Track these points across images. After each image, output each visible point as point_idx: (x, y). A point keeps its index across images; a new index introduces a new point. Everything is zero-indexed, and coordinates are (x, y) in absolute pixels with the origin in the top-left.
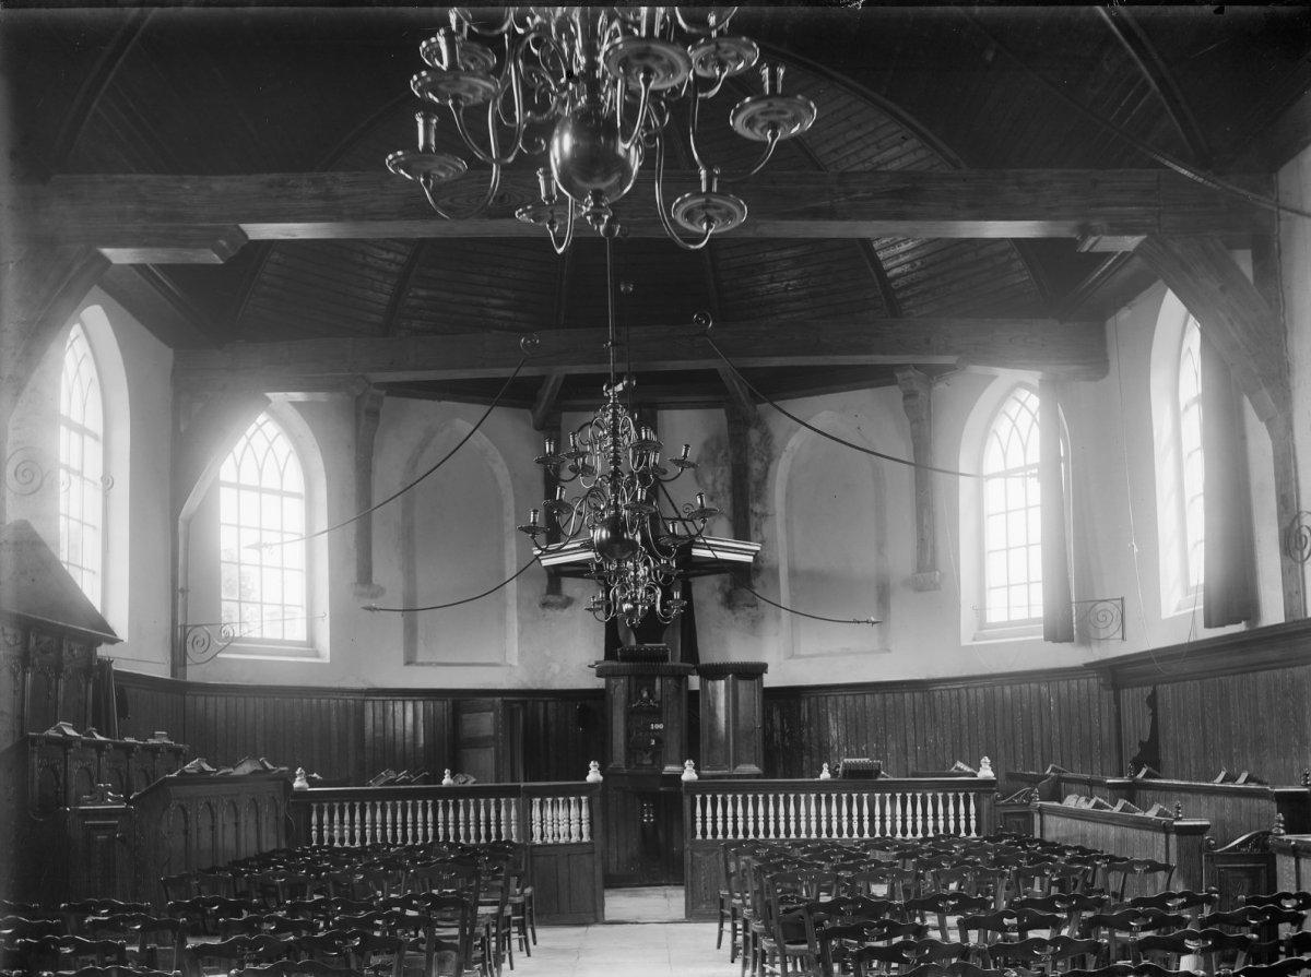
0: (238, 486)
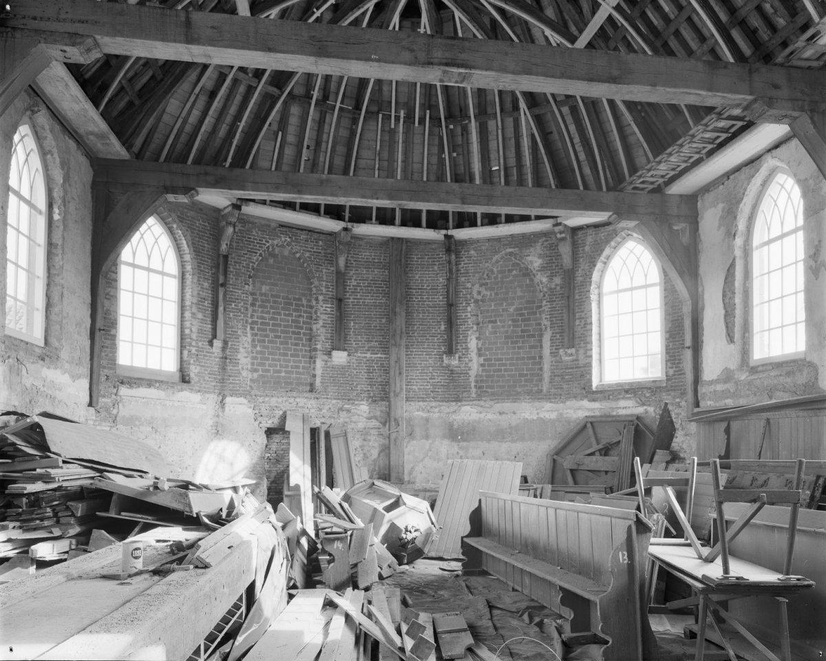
0: (134, 266)
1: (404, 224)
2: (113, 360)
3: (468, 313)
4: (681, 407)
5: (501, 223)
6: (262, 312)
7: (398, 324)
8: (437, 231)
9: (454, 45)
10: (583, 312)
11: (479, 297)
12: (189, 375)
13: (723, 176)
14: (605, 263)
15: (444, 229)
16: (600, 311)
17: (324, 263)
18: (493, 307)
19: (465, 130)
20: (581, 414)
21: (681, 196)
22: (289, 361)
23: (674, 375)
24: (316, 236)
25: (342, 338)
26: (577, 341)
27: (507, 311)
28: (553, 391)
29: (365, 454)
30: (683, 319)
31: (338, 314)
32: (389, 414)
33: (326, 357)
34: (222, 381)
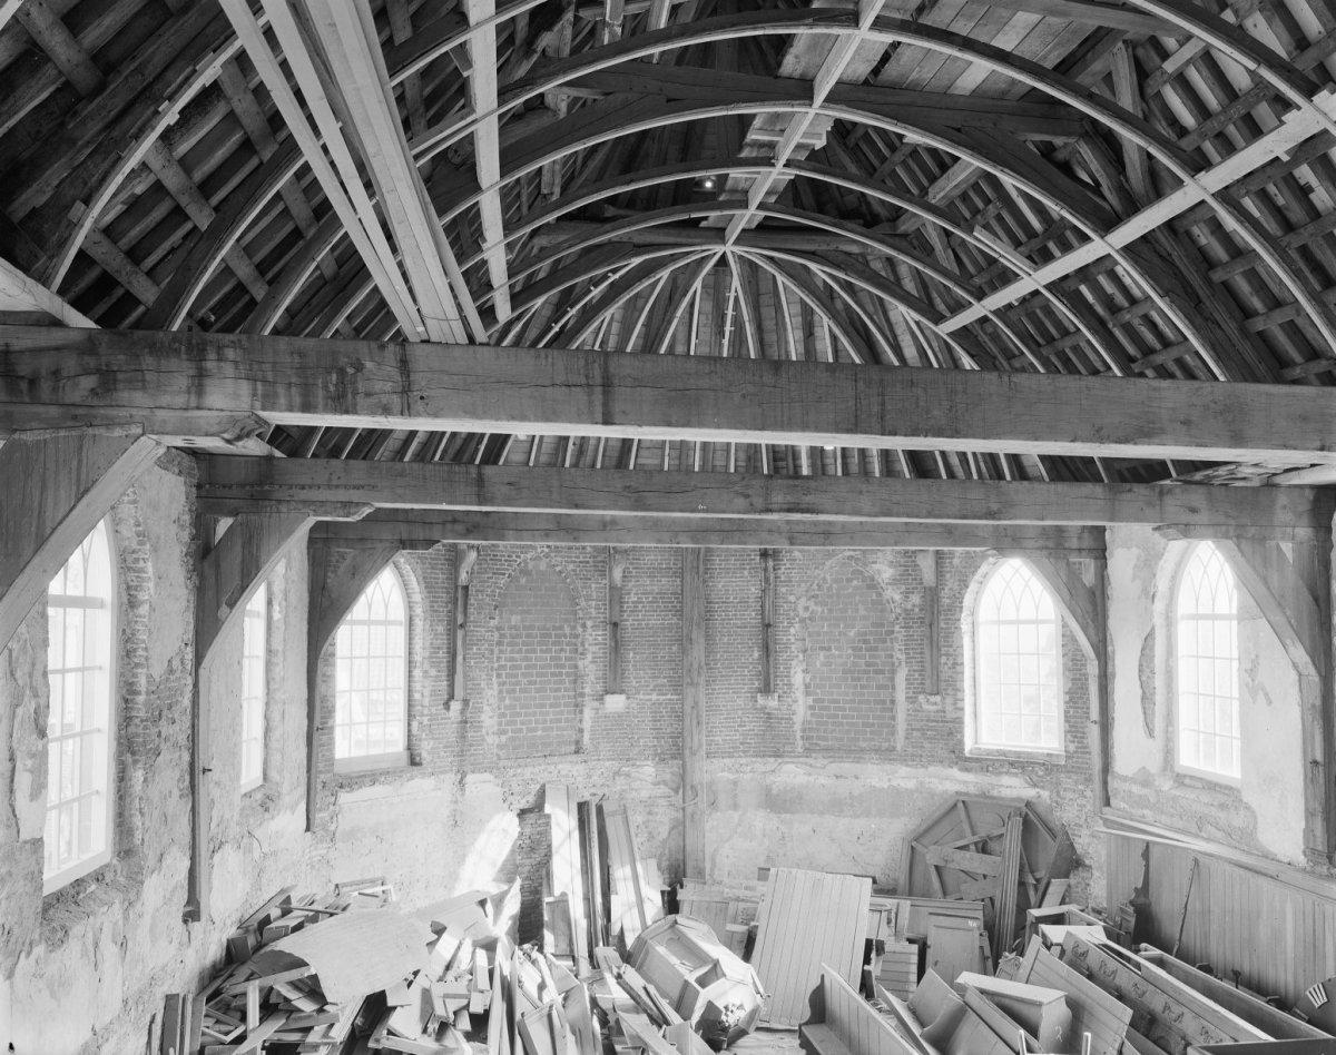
2: (331, 761)
3: (791, 635)
4: (1085, 797)
6: (512, 652)
7: (695, 654)
9: (797, 486)
10: (951, 646)
11: (807, 615)
12: (420, 755)
16: (974, 646)
18: (825, 629)
20: (951, 787)
22: (547, 713)
23: (1076, 752)
25: (619, 675)
26: (943, 685)
27: (845, 634)
28: (910, 750)
29: (650, 833)
30: (1087, 679)
31: (613, 644)
32: (683, 777)
33: (596, 704)
34: (461, 754)
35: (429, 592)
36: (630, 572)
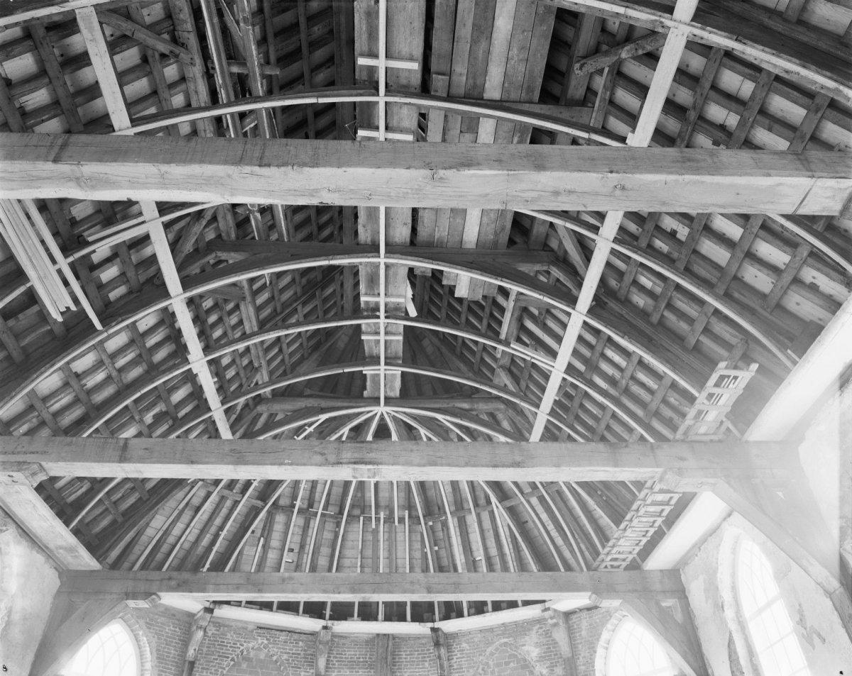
1: (388, 618)
5: (488, 612)
8: (422, 624)
9: (362, 447)
13: (694, 546)
14: (607, 649)
15: (430, 622)
17: (303, 665)
19: (445, 525)
21: (661, 571)
24: (296, 636)
35: (159, 662)
36: (334, 664)
